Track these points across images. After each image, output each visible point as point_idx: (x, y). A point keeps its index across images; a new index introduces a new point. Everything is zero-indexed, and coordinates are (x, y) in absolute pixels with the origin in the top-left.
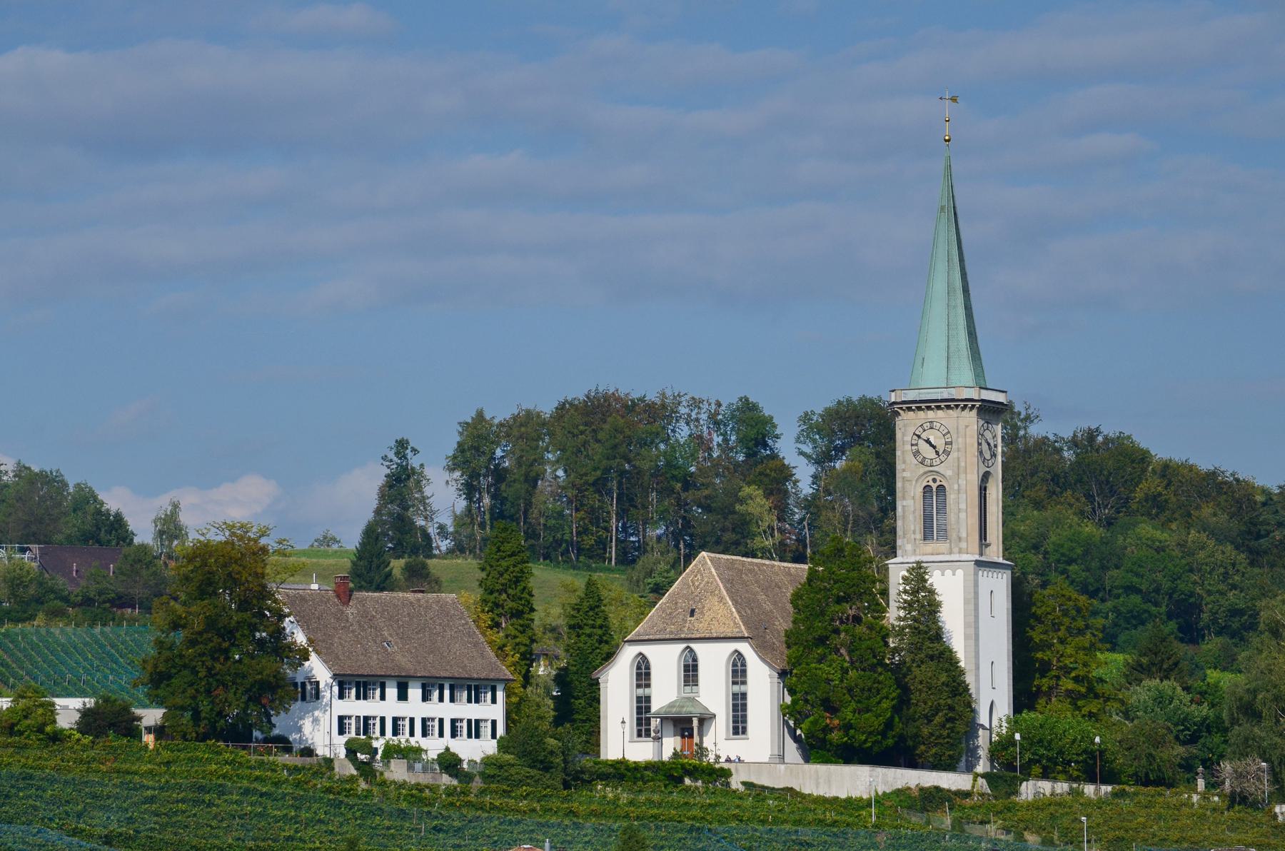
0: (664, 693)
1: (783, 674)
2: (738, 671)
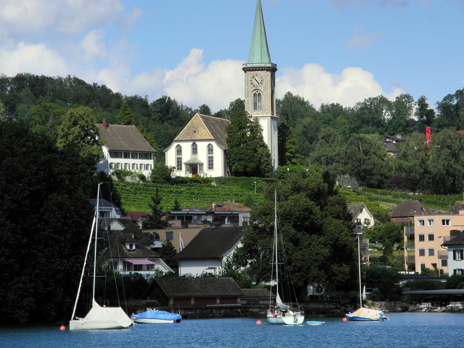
0: (187, 157)
1: (225, 152)
2: (210, 150)
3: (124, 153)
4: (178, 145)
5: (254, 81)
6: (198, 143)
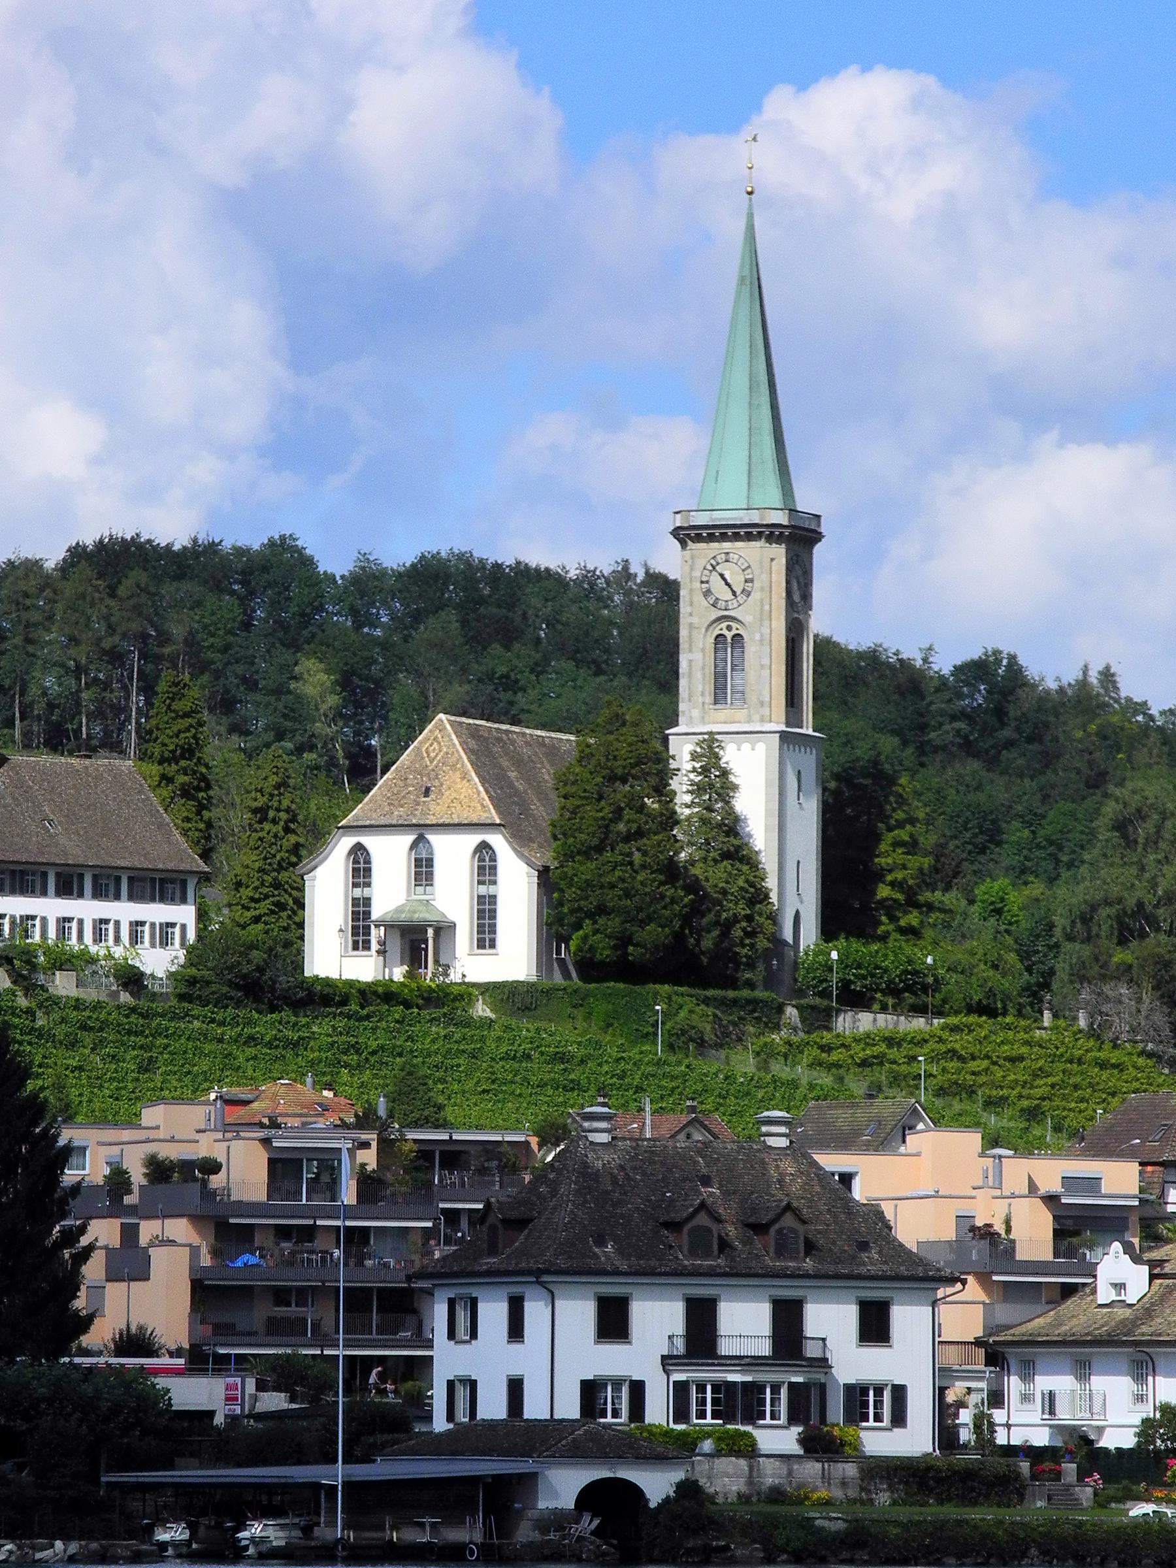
1: (544, 874)
3: (58, 875)
5: (717, 584)
6: (433, 838)
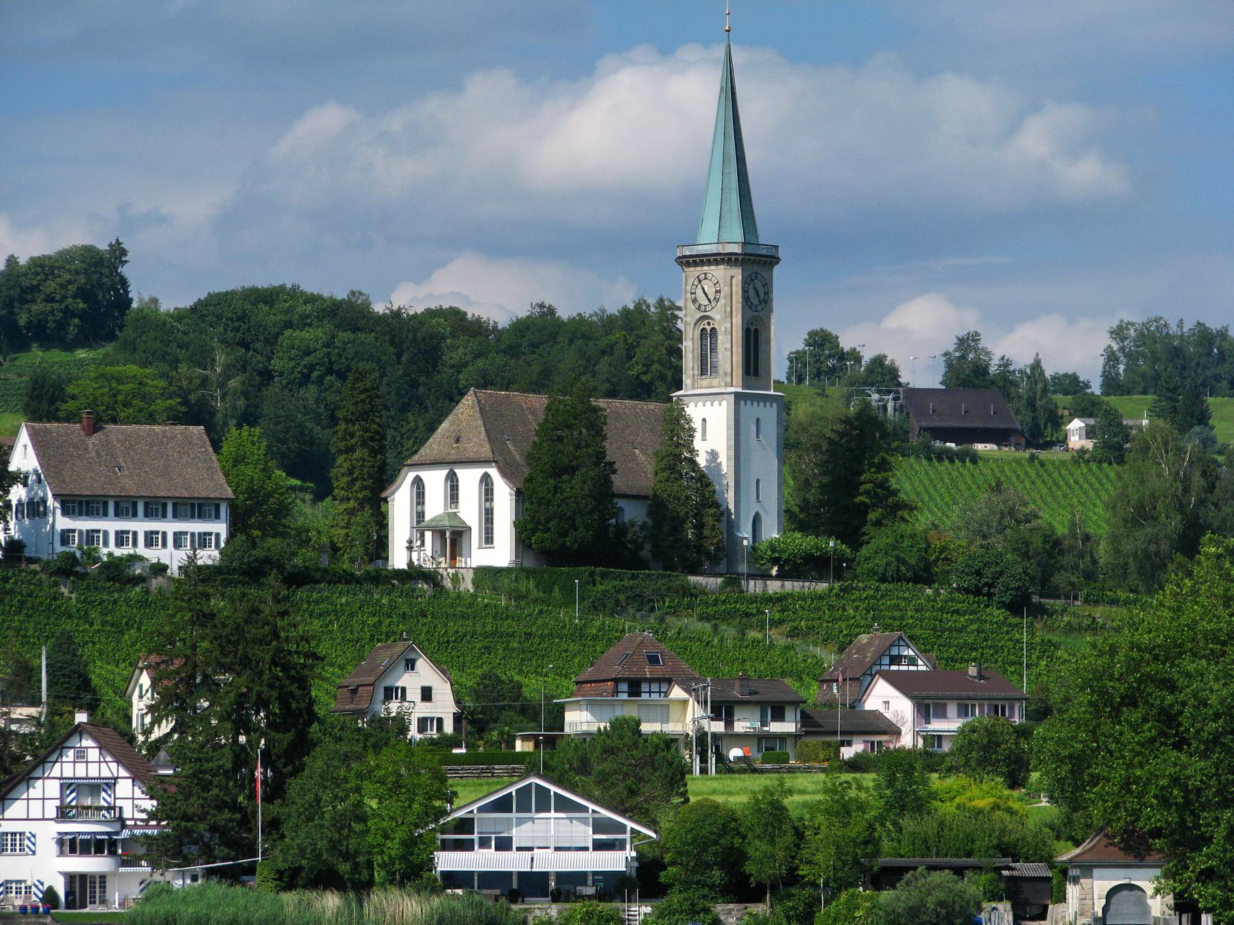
1: (519, 493)
4: (418, 477)
